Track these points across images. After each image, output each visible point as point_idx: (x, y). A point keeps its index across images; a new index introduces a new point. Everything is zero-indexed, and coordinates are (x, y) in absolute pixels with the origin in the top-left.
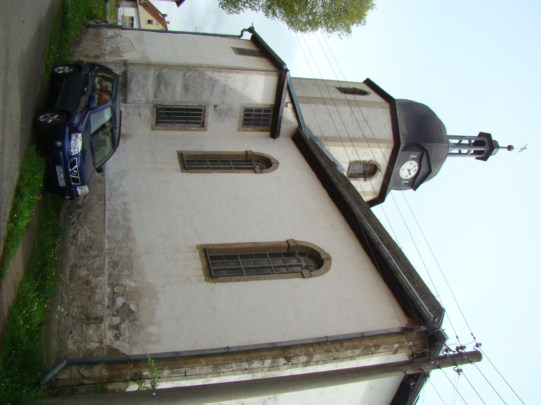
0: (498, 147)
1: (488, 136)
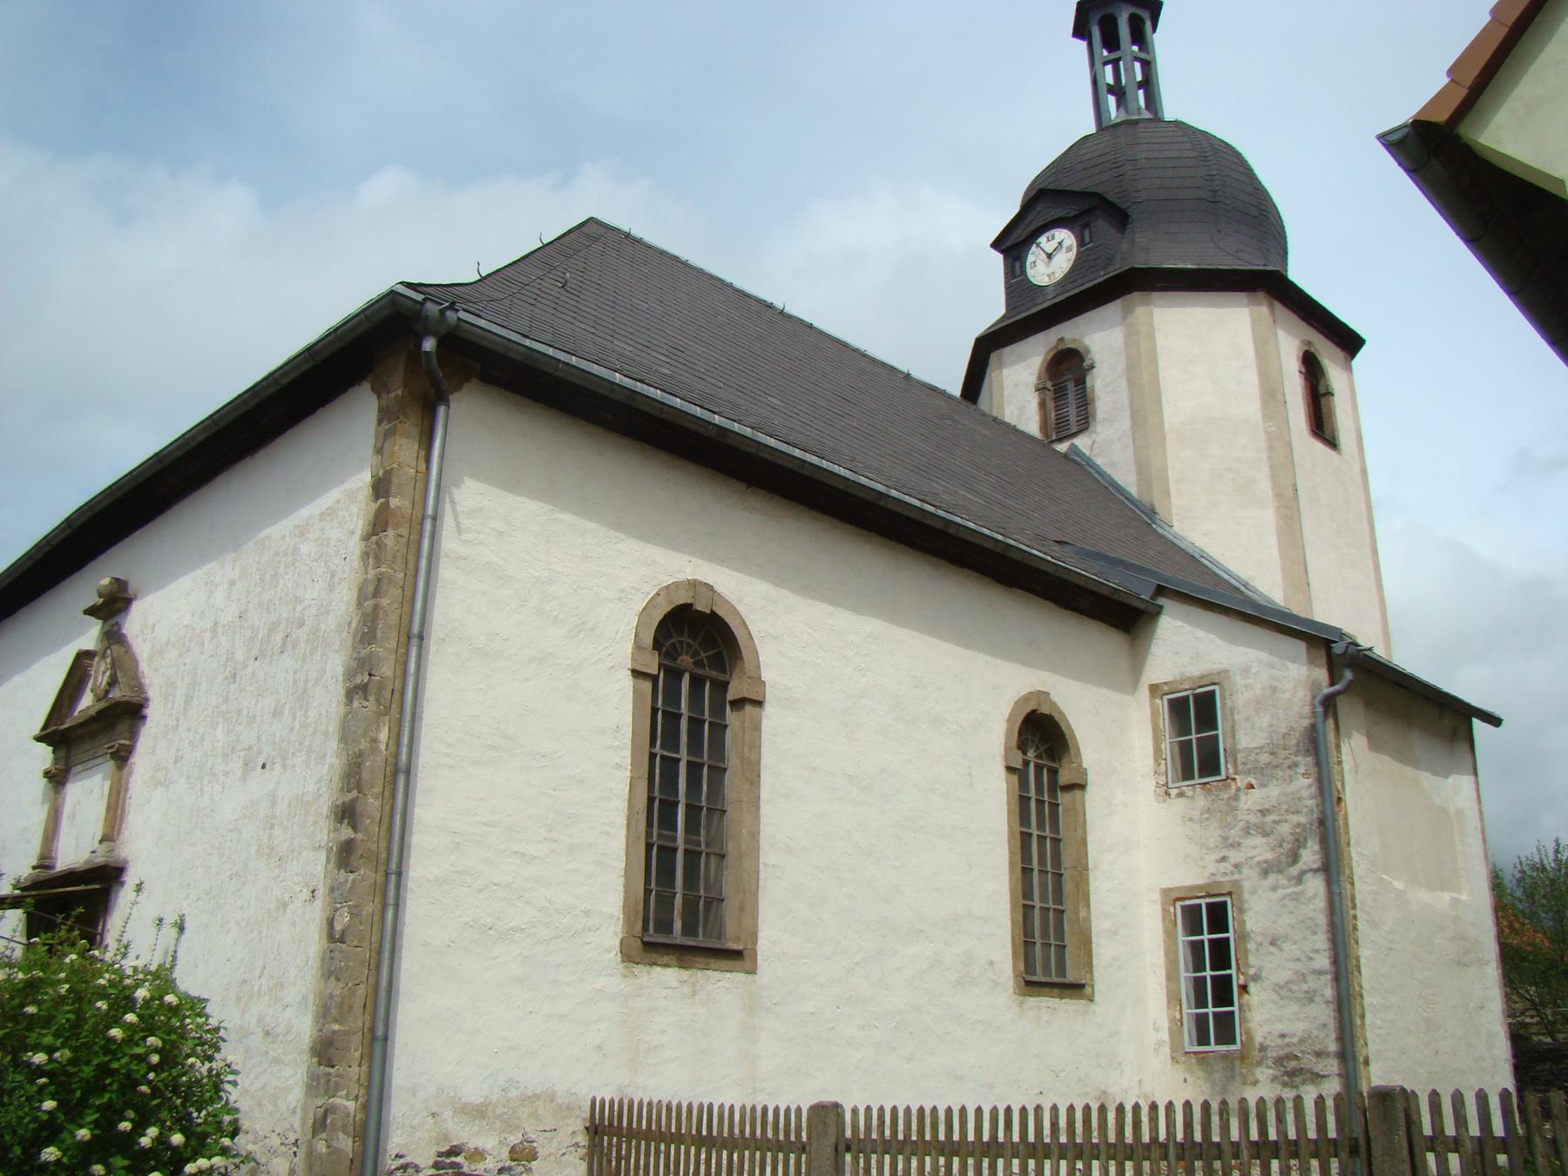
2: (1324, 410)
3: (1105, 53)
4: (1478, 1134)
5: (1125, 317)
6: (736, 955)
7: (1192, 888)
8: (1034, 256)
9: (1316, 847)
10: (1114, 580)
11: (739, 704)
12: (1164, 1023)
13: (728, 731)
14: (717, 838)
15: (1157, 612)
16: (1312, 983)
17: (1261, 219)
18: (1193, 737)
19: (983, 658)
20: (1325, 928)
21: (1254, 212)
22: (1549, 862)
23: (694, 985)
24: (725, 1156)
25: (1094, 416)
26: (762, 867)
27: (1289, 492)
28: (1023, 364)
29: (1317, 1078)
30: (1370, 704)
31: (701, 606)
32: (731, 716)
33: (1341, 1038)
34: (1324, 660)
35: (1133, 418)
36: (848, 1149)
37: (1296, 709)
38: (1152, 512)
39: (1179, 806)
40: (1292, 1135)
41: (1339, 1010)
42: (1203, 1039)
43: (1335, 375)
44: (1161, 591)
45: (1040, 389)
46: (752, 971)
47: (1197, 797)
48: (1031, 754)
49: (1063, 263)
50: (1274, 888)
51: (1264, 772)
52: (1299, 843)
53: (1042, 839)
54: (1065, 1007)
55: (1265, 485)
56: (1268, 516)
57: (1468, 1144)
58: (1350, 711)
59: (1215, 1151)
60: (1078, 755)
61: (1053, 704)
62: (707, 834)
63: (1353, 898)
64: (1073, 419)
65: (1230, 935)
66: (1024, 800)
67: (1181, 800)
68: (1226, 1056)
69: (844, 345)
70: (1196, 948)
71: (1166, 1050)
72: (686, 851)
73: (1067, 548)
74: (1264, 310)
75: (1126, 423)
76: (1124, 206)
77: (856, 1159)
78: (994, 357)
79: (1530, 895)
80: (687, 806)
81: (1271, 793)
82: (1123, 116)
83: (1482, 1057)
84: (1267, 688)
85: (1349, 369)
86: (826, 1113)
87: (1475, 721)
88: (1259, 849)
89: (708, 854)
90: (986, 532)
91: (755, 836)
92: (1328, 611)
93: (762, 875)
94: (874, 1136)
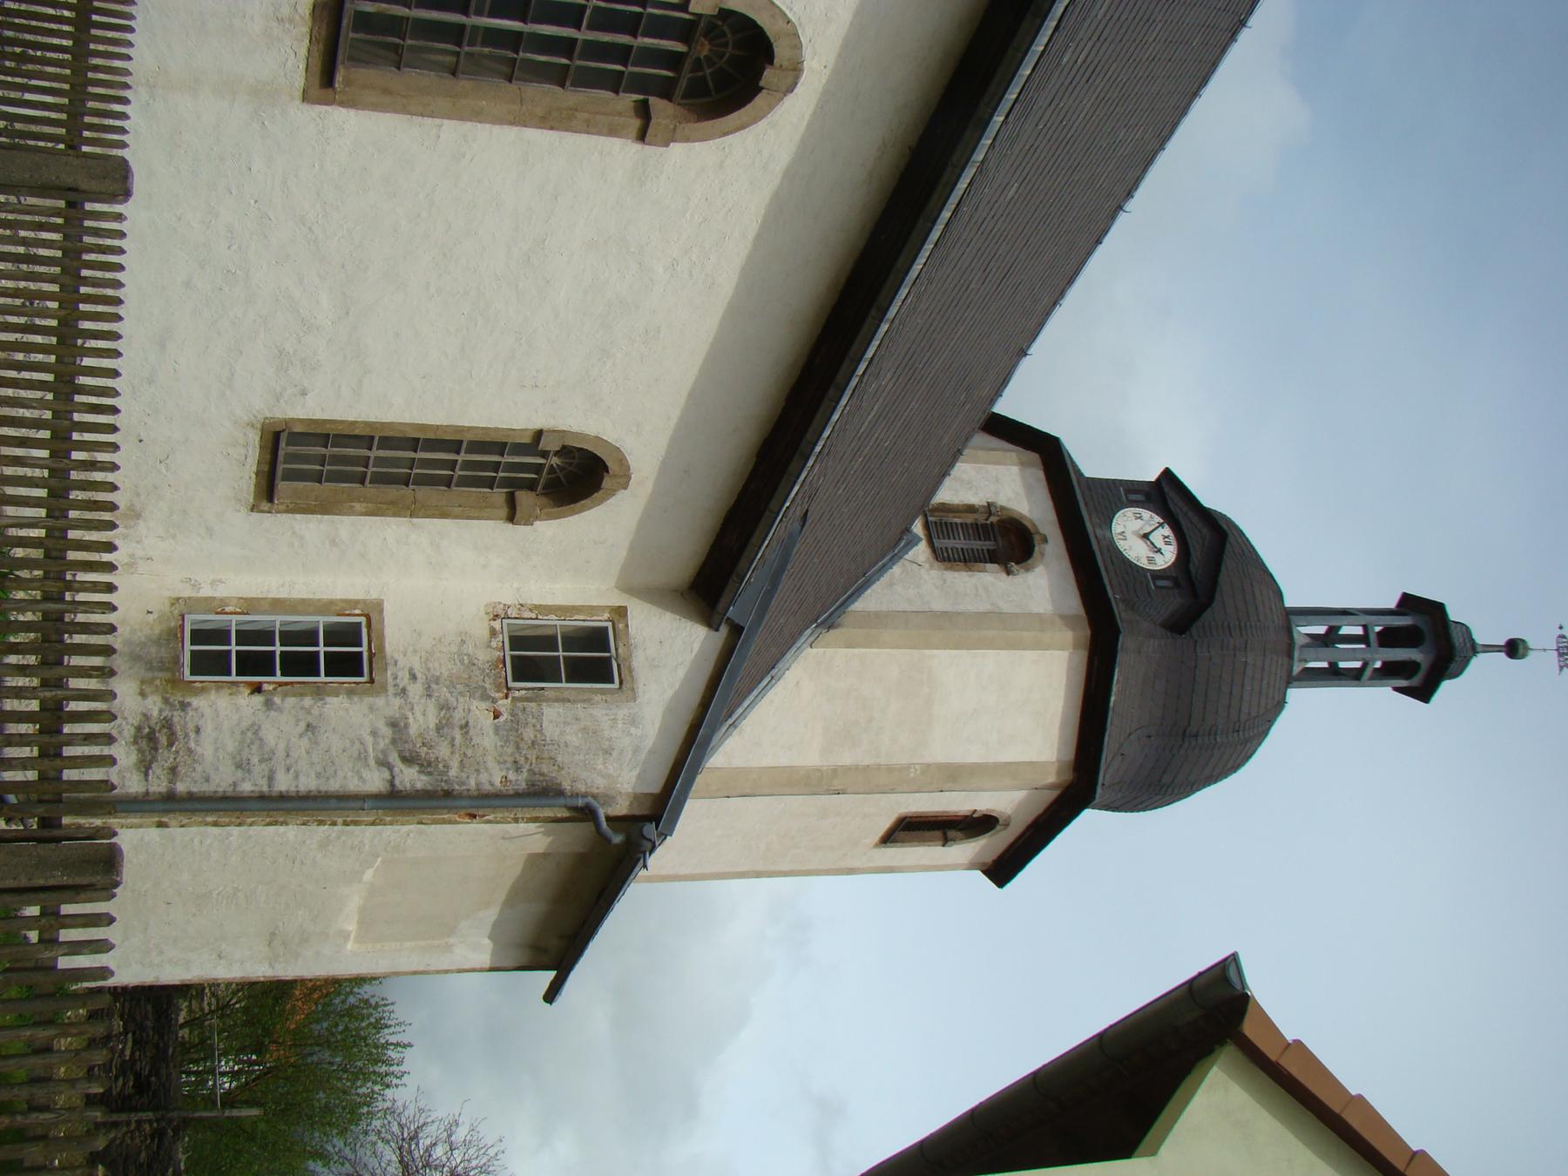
0: (1474, 649)
1: (1435, 610)
2: (928, 834)
3: (1378, 629)
4: (60, 966)
5: (1063, 617)
6: (328, 79)
7: (382, 637)
8: (1149, 518)
9: (419, 786)
10: (754, 577)
11: (644, 111)
12: (221, 592)
13: (610, 95)
14: (478, 69)
15: (711, 622)
16: (259, 770)
17: (1156, 786)
18: (561, 653)
19: (676, 414)
20: (323, 788)
21: (1166, 779)
22: (387, 1036)
23: (291, 21)
24: (65, 42)
25: (951, 569)
26: (437, 121)
27: (837, 784)
28: (1021, 491)
29: (145, 767)
30: (582, 860)
31: (769, 76)
32: (628, 100)
33: (191, 797)
34: (637, 812)
35: (944, 614)
36: (70, 205)
37: (584, 775)
38: (830, 625)
39: (481, 629)
40: (68, 751)
41: (225, 798)
42: (199, 636)
43: (967, 849)
44: (736, 630)
45: (989, 508)
46: (306, 97)
47: (488, 651)
48: (555, 461)
49: (1135, 552)
50: (374, 733)
51: (511, 731)
52: (425, 766)
53: (452, 465)
54: (245, 477)
55: (846, 758)
56: (811, 758)
57: (48, 954)
58: (575, 836)
59: (51, 658)
60: (550, 517)
61: (613, 492)
62: (482, 56)
63: (356, 823)
64: (949, 543)
65: (323, 678)
66: (500, 447)
67: (486, 633)
68: (176, 661)
69: (1070, 281)
70: (309, 636)
71: (187, 593)
72: (462, 27)
73: (797, 525)
74: (1051, 778)
75: (939, 605)
76: (1194, 630)
77: (57, 213)
78: (1034, 457)
79: (351, 1013)
80: (519, 34)
81: (487, 737)
82: (1299, 641)
83: (162, 952)
84: (609, 744)
85: (972, 866)
86: (118, 181)
87: (552, 974)
88: (423, 719)
89: (458, 54)
90: (826, 434)
91: (477, 116)
92: (697, 817)
93: (428, 121)
94: (86, 239)
